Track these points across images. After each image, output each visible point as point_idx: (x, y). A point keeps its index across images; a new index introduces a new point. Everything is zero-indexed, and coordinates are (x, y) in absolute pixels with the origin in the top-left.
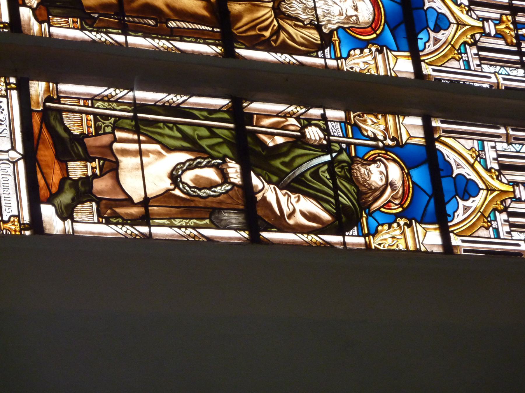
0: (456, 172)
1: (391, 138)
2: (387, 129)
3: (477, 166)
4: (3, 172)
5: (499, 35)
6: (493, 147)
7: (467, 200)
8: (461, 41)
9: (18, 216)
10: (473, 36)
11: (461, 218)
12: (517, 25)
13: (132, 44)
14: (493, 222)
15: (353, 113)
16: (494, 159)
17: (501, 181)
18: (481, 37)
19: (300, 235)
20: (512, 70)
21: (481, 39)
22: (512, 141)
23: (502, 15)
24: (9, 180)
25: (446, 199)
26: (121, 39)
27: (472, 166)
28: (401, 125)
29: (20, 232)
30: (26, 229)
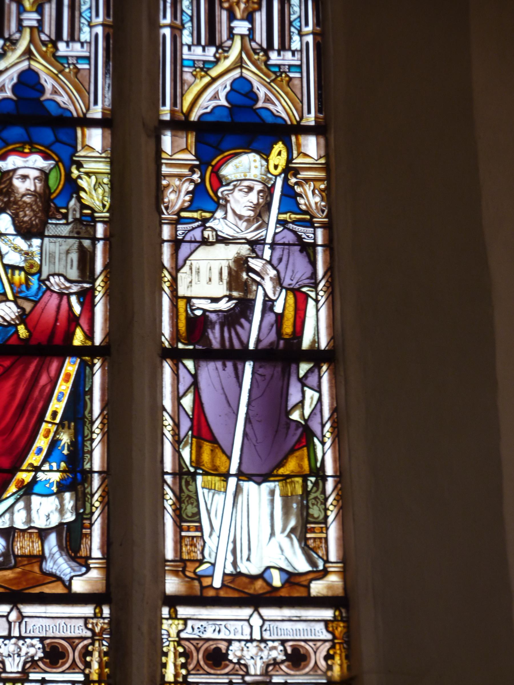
0: (223, 102)
2: (180, 176)
3: (214, 73)
4: (56, 630)
5: (250, 18)
8: (263, 67)
10: (44, 43)
11: (66, 98)
15: (164, 214)
16: (204, 50)
17: (230, 48)
18: (44, 33)
22: (178, 22)
23: (222, 7)
24: (41, 625)
27: (214, 80)
28: (172, 158)
29: (104, 618)
30: (101, 612)
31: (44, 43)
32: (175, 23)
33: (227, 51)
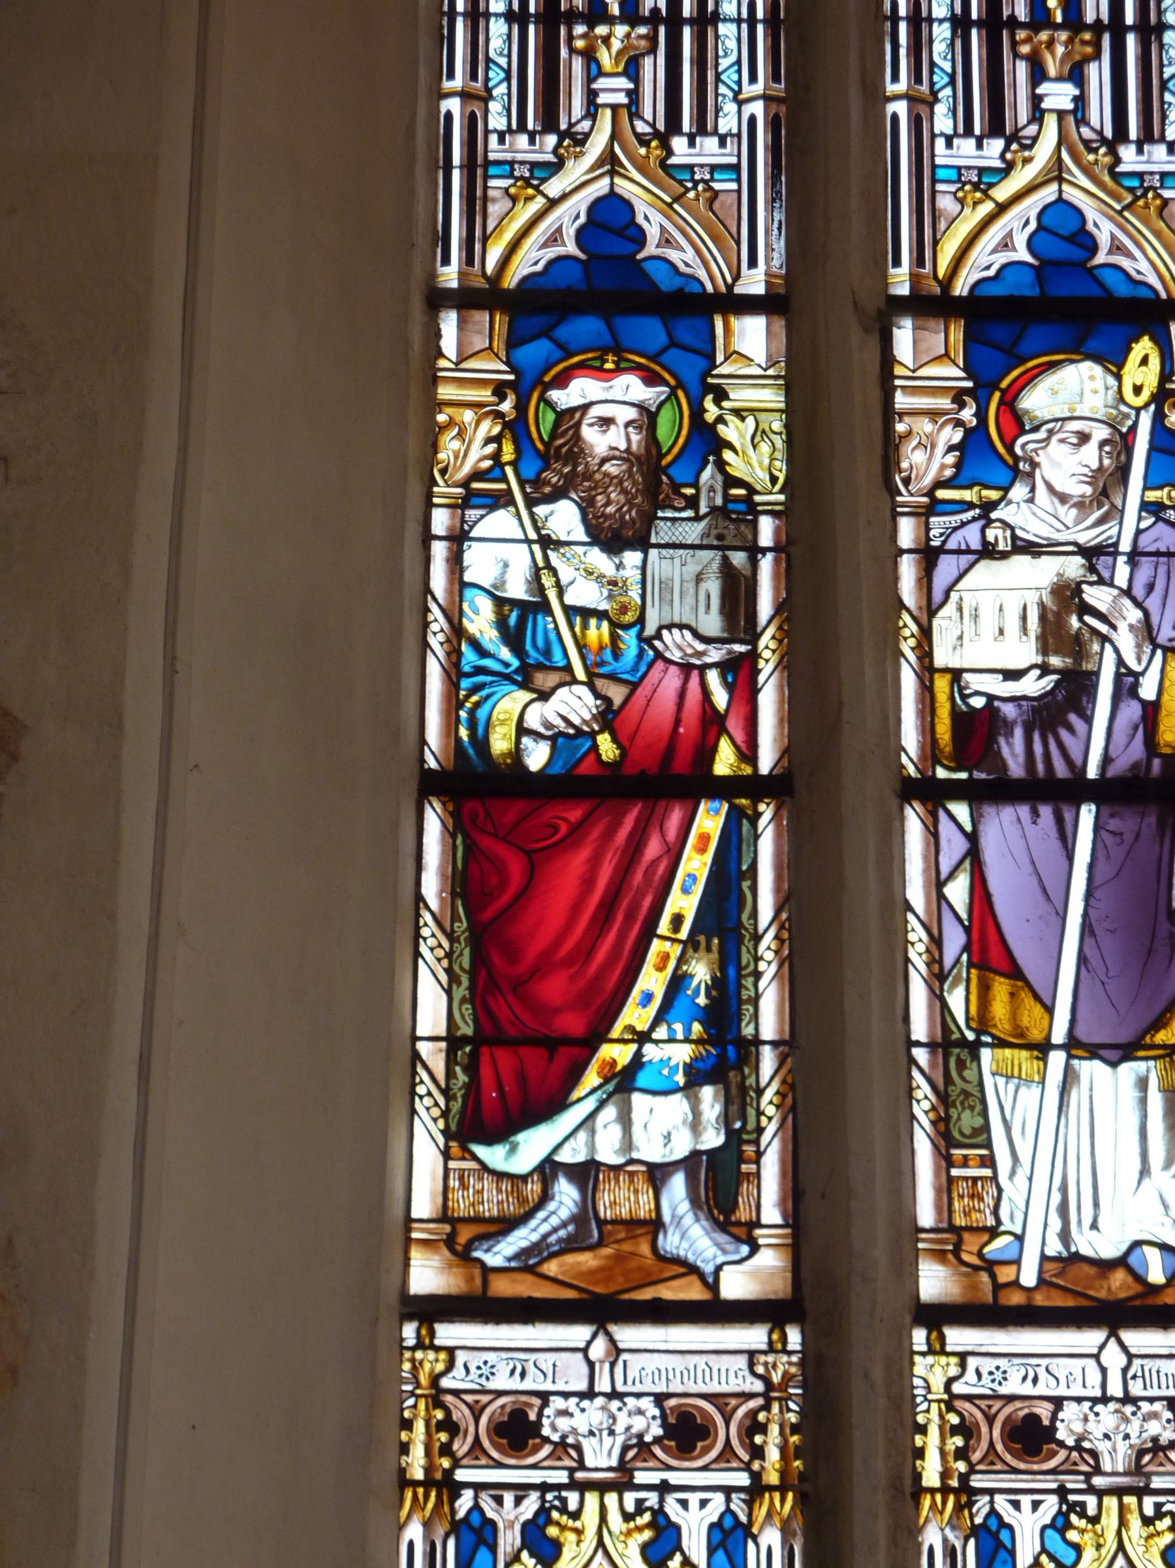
1: (955, 406)
3: (1002, 193)
4: (689, 1379)
6: (949, 144)
7: (642, 232)
8: (1107, 178)
9: (752, 1354)
10: (643, 140)
12: (1040, 18)
13: (781, 1030)
14: (697, 177)
17: (1035, 139)
18: (642, 119)
19: (762, 678)
20: (724, 51)
21: (645, 117)
23: (1016, 55)
25: (1096, 292)
26: (768, 1061)
29: (790, 1353)
30: (784, 1339)
31: (643, 140)
32: (918, 91)
33: (1030, 147)
